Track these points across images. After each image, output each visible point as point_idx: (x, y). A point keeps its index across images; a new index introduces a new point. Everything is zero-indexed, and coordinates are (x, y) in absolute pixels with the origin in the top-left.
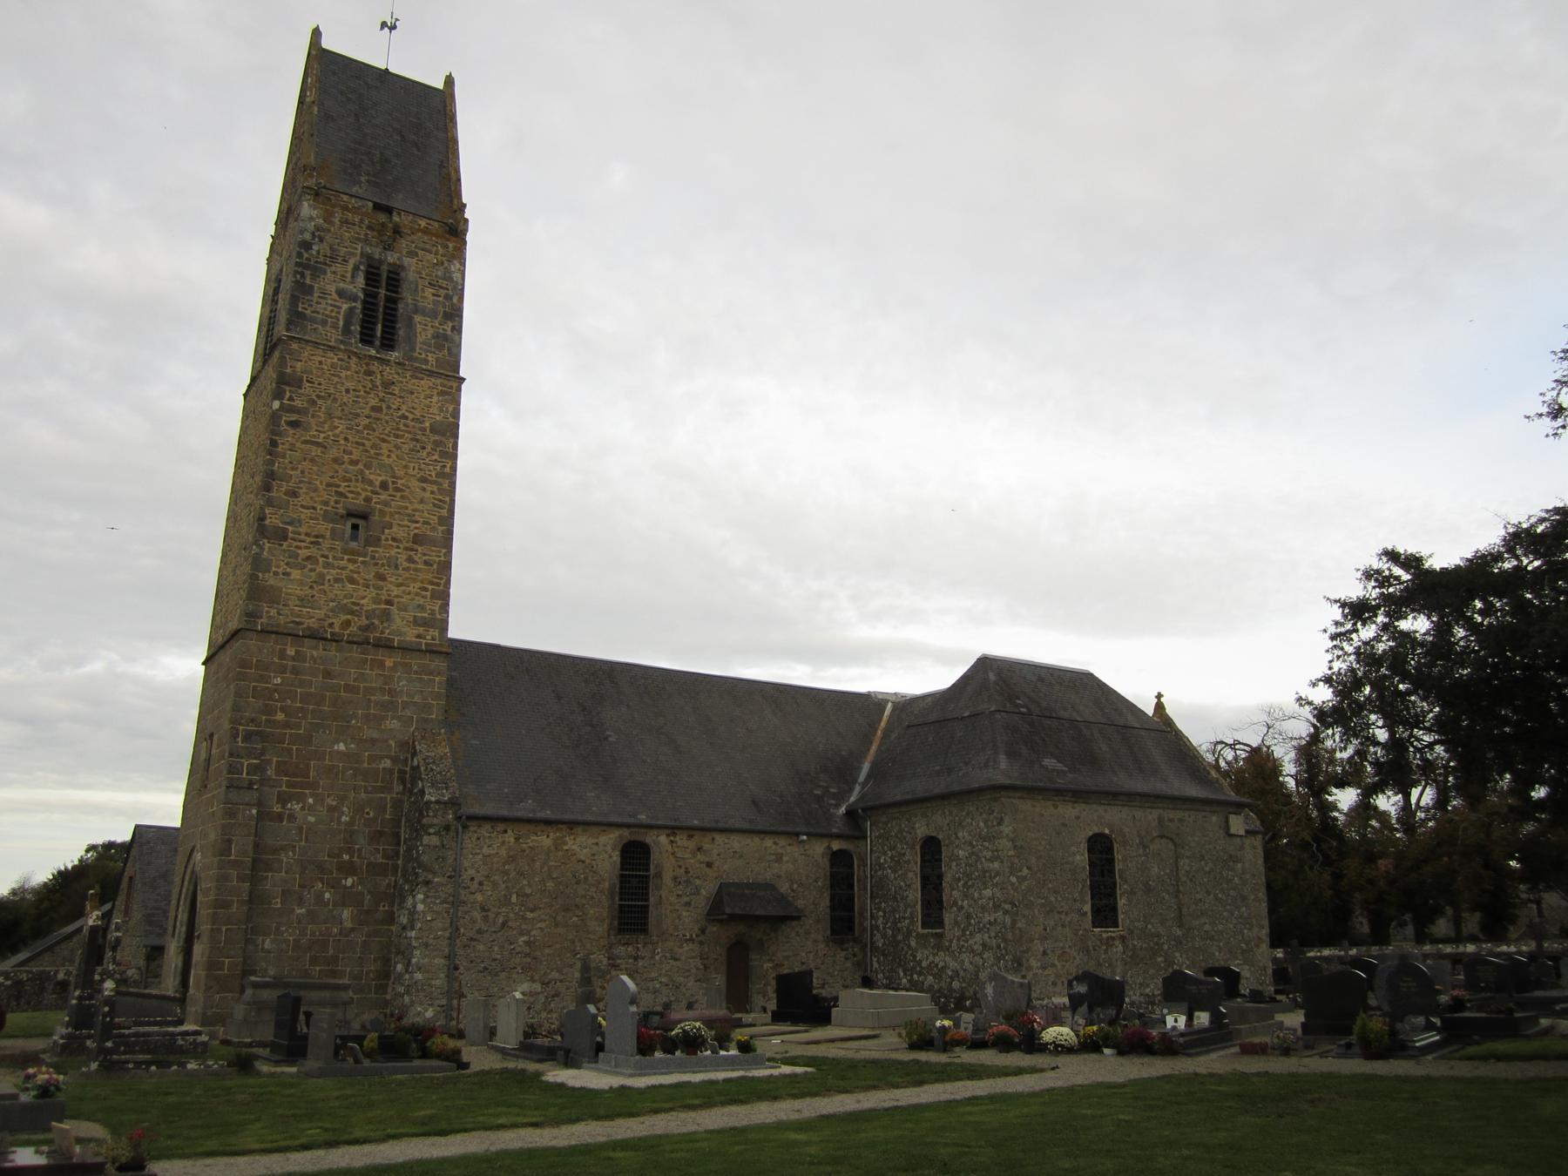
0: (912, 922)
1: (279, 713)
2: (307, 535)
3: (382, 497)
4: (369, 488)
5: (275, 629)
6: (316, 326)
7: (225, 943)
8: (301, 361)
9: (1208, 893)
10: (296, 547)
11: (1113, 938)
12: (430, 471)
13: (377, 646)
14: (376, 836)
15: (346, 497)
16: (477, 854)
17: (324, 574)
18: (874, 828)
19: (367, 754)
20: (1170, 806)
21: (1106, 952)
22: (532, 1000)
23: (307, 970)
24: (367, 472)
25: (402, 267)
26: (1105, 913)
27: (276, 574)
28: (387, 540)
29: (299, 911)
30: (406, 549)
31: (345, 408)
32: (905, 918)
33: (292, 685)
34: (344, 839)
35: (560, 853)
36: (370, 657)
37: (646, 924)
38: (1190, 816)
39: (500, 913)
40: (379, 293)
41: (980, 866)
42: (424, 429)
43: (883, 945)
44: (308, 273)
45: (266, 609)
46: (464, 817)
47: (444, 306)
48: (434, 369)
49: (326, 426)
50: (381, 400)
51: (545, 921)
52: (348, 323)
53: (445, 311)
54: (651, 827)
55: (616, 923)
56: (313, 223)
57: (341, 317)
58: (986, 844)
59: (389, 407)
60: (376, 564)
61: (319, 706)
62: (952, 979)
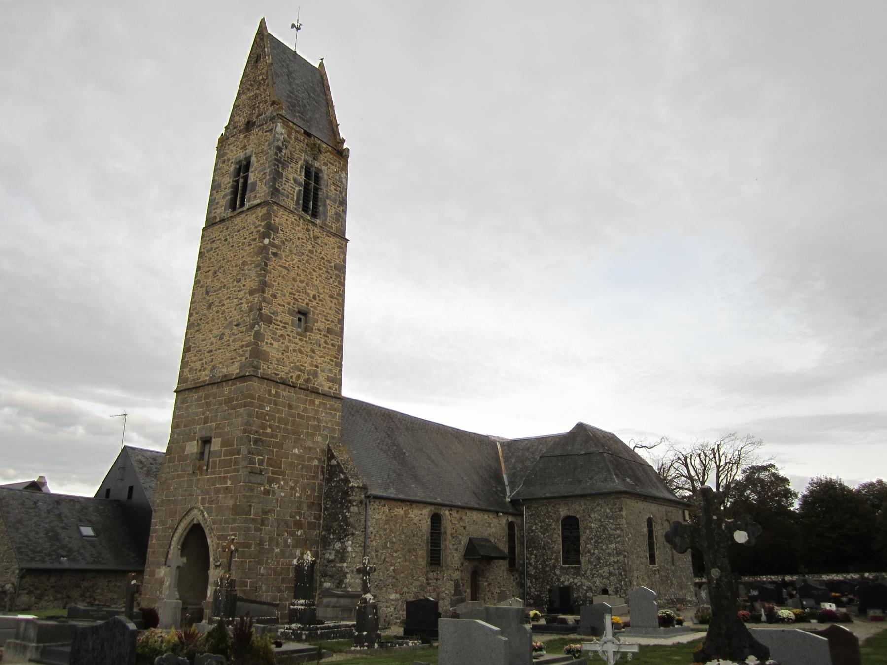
0: (557, 559)
1: (268, 429)
2: (281, 321)
3: (314, 304)
4: (308, 298)
5: (267, 377)
6: (284, 198)
7: (248, 570)
8: (278, 217)
10: (276, 328)
12: (334, 291)
13: (312, 392)
14: (311, 506)
15: (298, 302)
16: (373, 518)
17: (288, 346)
18: (528, 510)
19: (307, 456)
22: (396, 603)
23: (280, 586)
24: (307, 288)
25: (321, 171)
27: (267, 343)
28: (316, 329)
29: (276, 550)
30: (324, 336)
31: (298, 248)
32: (551, 559)
33: (274, 412)
34: (297, 507)
35: (407, 519)
36: (309, 398)
37: (439, 560)
39: (383, 553)
40: (311, 184)
41: (606, 532)
42: (331, 267)
43: (534, 573)
44: (280, 165)
45: (262, 364)
46: (372, 497)
47: (339, 197)
48: (335, 232)
49: (289, 258)
50: (313, 247)
51: (401, 558)
52: (298, 199)
53: (339, 200)
55: (429, 559)
56: (283, 137)
57: (295, 194)
58: (611, 521)
59: (316, 252)
60: (311, 343)
61: (286, 425)
62: (587, 591)
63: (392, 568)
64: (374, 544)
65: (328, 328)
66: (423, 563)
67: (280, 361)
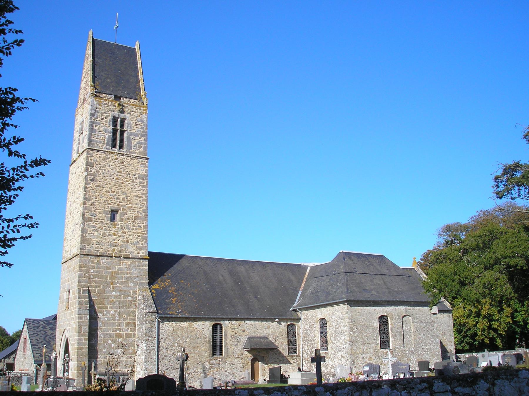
9: (424, 335)
10: (95, 224)
35: (191, 328)
45: (87, 246)
65: (135, 217)
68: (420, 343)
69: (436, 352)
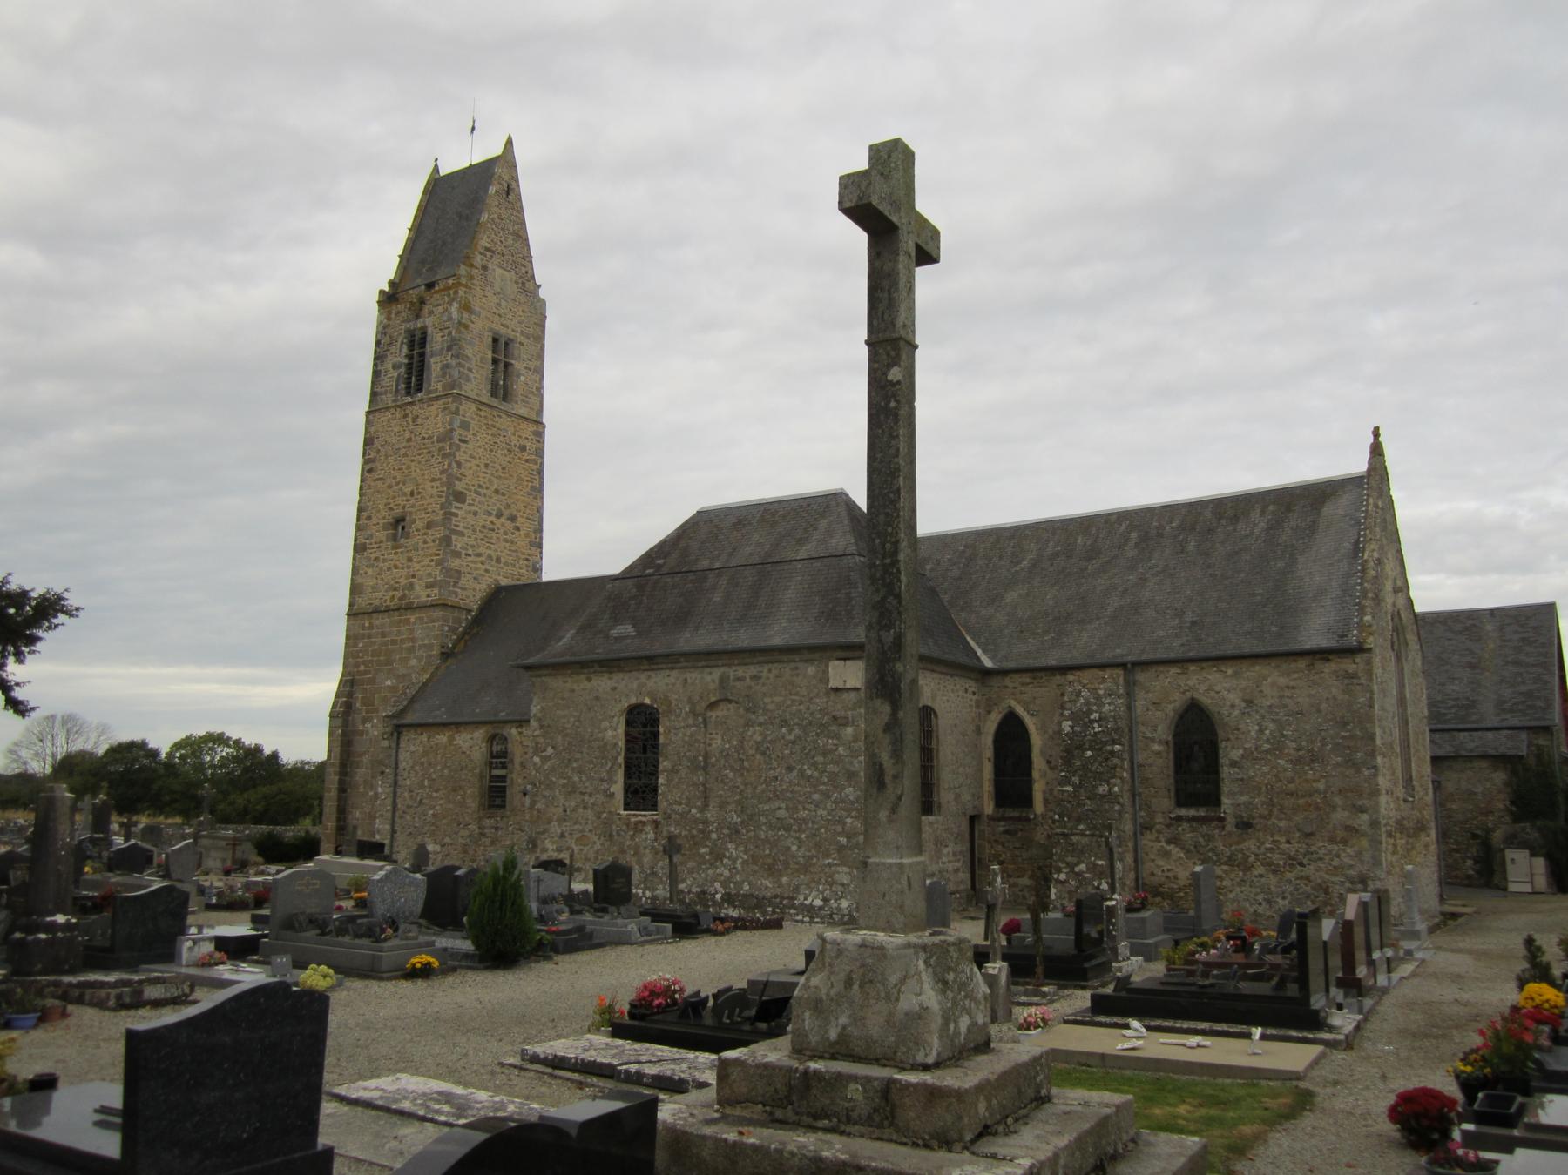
9: (790, 769)
11: (643, 823)
13: (406, 609)
20: (736, 662)
21: (632, 838)
26: (641, 793)
38: (770, 671)
54: (505, 722)
63: (431, 812)
64: (408, 782)
66: (473, 805)
67: (374, 588)
68: (770, 799)
69: (840, 834)
